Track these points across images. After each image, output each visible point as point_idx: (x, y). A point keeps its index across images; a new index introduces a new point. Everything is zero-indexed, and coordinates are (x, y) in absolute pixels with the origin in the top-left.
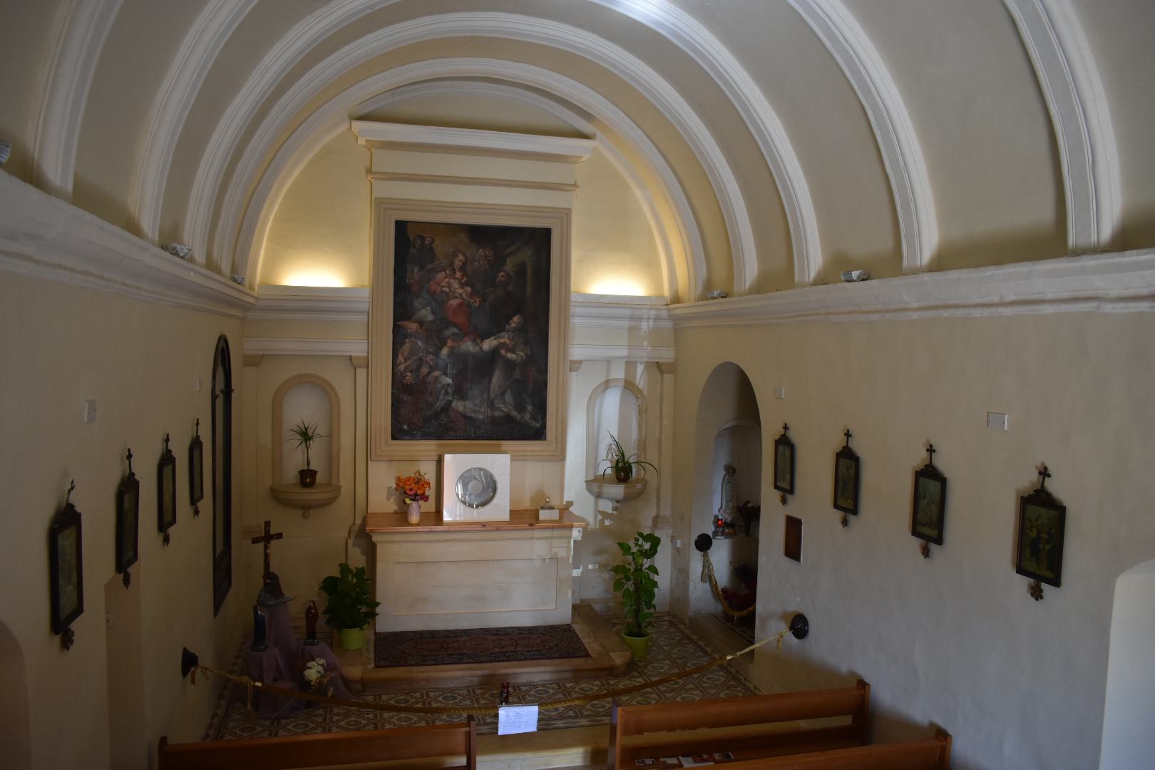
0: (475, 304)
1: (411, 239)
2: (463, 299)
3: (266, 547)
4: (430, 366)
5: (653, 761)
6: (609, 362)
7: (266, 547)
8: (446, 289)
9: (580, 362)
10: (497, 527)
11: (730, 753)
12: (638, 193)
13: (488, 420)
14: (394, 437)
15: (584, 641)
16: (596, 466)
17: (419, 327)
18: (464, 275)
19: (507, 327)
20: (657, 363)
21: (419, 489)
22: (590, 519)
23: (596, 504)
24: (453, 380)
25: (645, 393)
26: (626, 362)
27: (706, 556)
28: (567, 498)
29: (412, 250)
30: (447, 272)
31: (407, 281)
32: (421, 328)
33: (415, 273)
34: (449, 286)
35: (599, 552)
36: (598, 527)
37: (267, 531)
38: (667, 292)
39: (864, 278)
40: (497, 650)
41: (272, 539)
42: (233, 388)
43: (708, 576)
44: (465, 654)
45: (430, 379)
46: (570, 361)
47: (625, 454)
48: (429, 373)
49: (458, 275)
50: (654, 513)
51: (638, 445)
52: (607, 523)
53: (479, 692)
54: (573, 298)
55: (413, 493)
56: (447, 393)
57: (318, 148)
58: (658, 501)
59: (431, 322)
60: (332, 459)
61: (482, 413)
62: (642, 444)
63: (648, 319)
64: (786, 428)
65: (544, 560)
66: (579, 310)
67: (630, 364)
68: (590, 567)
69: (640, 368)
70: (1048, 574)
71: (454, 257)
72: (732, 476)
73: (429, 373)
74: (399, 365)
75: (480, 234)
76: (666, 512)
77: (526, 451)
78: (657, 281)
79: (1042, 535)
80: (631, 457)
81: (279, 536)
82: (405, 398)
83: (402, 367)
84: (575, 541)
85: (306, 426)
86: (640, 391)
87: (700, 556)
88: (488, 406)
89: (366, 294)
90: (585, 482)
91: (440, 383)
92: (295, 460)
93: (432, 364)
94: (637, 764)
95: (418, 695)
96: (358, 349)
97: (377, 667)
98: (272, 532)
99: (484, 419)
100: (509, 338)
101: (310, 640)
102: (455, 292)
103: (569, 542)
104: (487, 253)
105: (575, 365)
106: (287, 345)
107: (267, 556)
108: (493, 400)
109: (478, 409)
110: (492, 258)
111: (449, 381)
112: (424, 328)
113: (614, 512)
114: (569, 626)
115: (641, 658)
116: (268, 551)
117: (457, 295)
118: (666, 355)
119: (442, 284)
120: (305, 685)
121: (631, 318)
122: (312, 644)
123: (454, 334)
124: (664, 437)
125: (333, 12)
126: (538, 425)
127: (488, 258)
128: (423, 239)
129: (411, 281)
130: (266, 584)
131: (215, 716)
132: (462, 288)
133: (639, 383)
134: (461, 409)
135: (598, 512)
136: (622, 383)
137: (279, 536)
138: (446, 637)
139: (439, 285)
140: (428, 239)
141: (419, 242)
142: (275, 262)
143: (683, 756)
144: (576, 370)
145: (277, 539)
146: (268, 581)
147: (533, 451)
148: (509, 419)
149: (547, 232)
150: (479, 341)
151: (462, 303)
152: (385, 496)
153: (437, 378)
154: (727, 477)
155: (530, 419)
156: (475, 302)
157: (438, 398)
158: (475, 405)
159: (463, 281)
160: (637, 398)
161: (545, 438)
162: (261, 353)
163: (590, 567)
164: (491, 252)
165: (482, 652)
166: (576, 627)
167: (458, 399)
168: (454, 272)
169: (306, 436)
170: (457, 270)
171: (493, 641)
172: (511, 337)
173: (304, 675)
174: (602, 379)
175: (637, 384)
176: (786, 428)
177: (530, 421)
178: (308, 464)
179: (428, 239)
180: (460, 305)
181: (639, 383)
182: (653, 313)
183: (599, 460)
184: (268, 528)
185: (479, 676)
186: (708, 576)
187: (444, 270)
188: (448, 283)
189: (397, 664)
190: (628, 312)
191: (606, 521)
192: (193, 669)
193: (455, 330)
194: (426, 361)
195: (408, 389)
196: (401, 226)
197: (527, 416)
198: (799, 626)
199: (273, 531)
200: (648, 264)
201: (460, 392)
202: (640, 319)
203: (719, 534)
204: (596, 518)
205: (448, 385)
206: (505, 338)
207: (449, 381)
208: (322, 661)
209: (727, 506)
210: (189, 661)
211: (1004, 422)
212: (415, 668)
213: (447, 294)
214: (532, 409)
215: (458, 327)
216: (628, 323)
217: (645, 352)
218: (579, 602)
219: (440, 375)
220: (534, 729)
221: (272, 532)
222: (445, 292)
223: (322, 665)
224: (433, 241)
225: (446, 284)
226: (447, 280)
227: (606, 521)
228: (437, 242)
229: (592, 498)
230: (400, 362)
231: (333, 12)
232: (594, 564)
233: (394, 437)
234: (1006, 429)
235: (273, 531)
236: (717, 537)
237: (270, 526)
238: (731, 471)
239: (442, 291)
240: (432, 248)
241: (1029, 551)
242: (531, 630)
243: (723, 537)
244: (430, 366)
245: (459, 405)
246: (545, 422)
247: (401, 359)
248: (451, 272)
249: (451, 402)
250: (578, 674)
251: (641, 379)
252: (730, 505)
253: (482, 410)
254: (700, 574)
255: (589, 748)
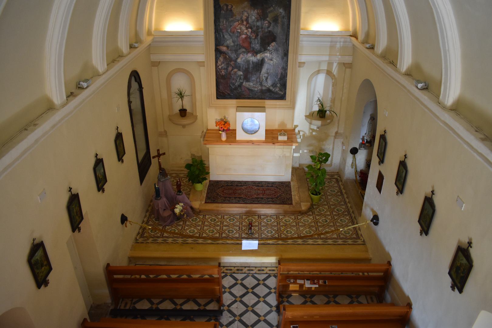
0: (253, 37)
1: (222, 6)
2: (247, 35)
4: (233, 67)
5: (294, 281)
6: (320, 63)
8: (239, 31)
9: (304, 63)
10: (259, 143)
11: (327, 281)
13: (259, 91)
17: (227, 49)
18: (248, 23)
21: (225, 127)
23: (310, 126)
28: (295, 123)
29: (223, 12)
30: (239, 22)
31: (221, 27)
32: (228, 49)
33: (223, 23)
34: (241, 29)
35: (310, 145)
37: (158, 153)
38: (351, 29)
39: (422, 89)
40: (255, 196)
41: (161, 156)
43: (354, 164)
44: (242, 198)
46: (299, 63)
48: (232, 70)
49: (245, 23)
51: (331, 100)
52: (314, 133)
53: (244, 217)
54: (302, 32)
55: (222, 129)
56: (240, 79)
58: (338, 123)
59: (232, 46)
60: (193, 104)
61: (257, 88)
62: (333, 101)
63: (340, 42)
64: (385, 132)
65: (280, 157)
66: (305, 39)
67: (330, 64)
68: (305, 151)
69: (335, 65)
70: (459, 285)
71: (242, 14)
72: (372, 121)
73: (232, 70)
76: (341, 131)
77: (276, 105)
78: (346, 23)
79: (461, 268)
80: (327, 108)
81: (164, 154)
84: (293, 149)
85: (181, 91)
86: (334, 75)
87: (352, 156)
89: (202, 33)
90: (305, 116)
91: (237, 74)
92: (177, 105)
94: (287, 282)
95: (220, 217)
97: (205, 203)
98: (161, 153)
99: (257, 90)
103: (291, 150)
104: (258, 11)
105: (302, 64)
106: (168, 57)
107: (159, 162)
109: (255, 86)
110: (261, 14)
112: (229, 49)
113: (318, 129)
115: (316, 203)
116: (160, 161)
117: (244, 33)
118: (348, 59)
119: (237, 28)
120: (174, 214)
122: (179, 195)
124: (343, 98)
126: (282, 93)
127: (259, 14)
128: (227, 6)
129: (222, 27)
130: (160, 172)
131: (146, 216)
132: (247, 30)
134: (247, 86)
136: (325, 71)
137: (164, 154)
138: (237, 186)
140: (230, 6)
141: (225, 7)
143: (307, 280)
146: (161, 171)
147: (280, 105)
148: (269, 90)
150: (255, 55)
151: (247, 37)
153: (236, 72)
154: (370, 121)
155: (279, 90)
156: (253, 36)
157: (236, 81)
159: (247, 26)
160: (332, 79)
162: (159, 61)
163: (305, 151)
164: (261, 11)
165: (249, 197)
166: (292, 184)
167: (246, 82)
168: (243, 22)
170: (244, 21)
171: (255, 190)
173: (174, 211)
174: (317, 69)
175: (333, 72)
176: (385, 132)
177: (278, 91)
178: (183, 107)
179: (230, 6)
180: (246, 38)
181: (334, 72)
182: (342, 40)
184: (159, 152)
185: (245, 210)
187: (238, 21)
189: (214, 202)
190: (329, 39)
191: (313, 133)
192: (126, 222)
193: (244, 50)
195: (223, 77)
197: (277, 90)
198: (376, 219)
200: (343, 13)
201: (247, 79)
202: (336, 42)
203: (363, 147)
205: (241, 75)
208: (182, 204)
209: (368, 134)
210: (124, 219)
211: (462, 206)
212: (220, 205)
213: (240, 33)
214: (280, 86)
215: (245, 49)
217: (337, 59)
218: (298, 166)
219: (237, 71)
220: (257, 248)
221: (161, 153)
222: (239, 32)
223: (182, 206)
224: (232, 7)
226: (239, 26)
227: (313, 133)
228: (234, 7)
229: (308, 124)
230: (219, 65)
232: (307, 150)
233: (217, 98)
234: (462, 210)
236: (361, 149)
237: (159, 151)
238: (372, 119)
239: (237, 31)
240: (232, 10)
241: (455, 269)
242: (273, 183)
243: (364, 149)
244: (233, 67)
245: (246, 84)
246: (286, 92)
247: (219, 63)
249: (242, 83)
250: (286, 213)
252: (370, 133)
255: (278, 258)
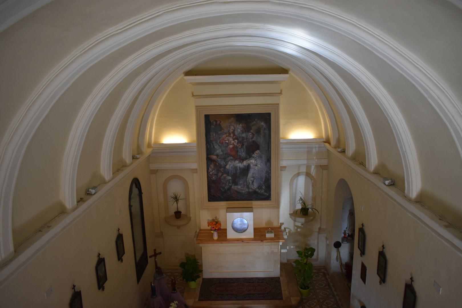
0: (239, 147)
1: (211, 122)
3: (155, 259)
4: (222, 173)
6: (299, 166)
7: (155, 259)
8: (227, 142)
9: (285, 167)
10: (248, 240)
12: (310, 93)
14: (209, 201)
15: (282, 289)
16: (295, 206)
17: (217, 157)
18: (234, 135)
19: (253, 155)
20: (321, 165)
22: (292, 229)
23: (294, 223)
24: (231, 177)
25: (315, 177)
26: (307, 166)
27: (338, 252)
29: (213, 127)
30: (227, 134)
32: (218, 157)
33: (213, 135)
36: (295, 232)
37: (155, 253)
38: (324, 136)
42: (142, 192)
43: (339, 258)
45: (222, 177)
46: (281, 167)
47: (306, 203)
49: (232, 135)
50: (319, 226)
52: (299, 230)
54: (281, 141)
55: (214, 229)
56: (229, 182)
57: (171, 87)
60: (187, 206)
61: (245, 190)
62: (314, 199)
67: (308, 167)
68: (292, 247)
69: (313, 167)
74: (210, 173)
75: (240, 118)
81: (160, 253)
82: (213, 185)
83: (211, 173)
84: (280, 245)
85: (176, 195)
86: (313, 177)
88: (246, 187)
89: (195, 144)
90: (289, 214)
92: (173, 208)
93: (223, 172)
96: (194, 166)
97: (199, 300)
99: (245, 192)
100: (254, 160)
101: (173, 291)
102: (231, 142)
103: (279, 247)
104: (243, 125)
105: (283, 168)
108: (248, 185)
109: (242, 189)
111: (230, 178)
112: (219, 157)
113: (302, 226)
114: (279, 278)
116: (156, 260)
117: (232, 143)
118: (324, 162)
119: (225, 139)
121: (308, 148)
122: (174, 293)
123: (231, 159)
125: (149, 73)
128: (216, 121)
130: (156, 271)
132: (234, 140)
133: (313, 173)
134: (236, 189)
135: (295, 226)
136: (305, 173)
137: (160, 253)
139: (224, 140)
141: (215, 123)
142: (159, 133)
144: (284, 170)
145: (159, 254)
148: (255, 192)
149: (269, 114)
152: (207, 225)
153: (225, 177)
154: (350, 216)
157: (226, 185)
158: (241, 187)
159: (234, 137)
160: (312, 180)
161: (271, 199)
163: (292, 247)
167: (234, 185)
168: (230, 134)
169: (176, 199)
170: (231, 133)
172: (255, 159)
174: (297, 172)
175: (311, 174)
177: (264, 193)
179: (218, 121)
180: (233, 148)
181: (313, 173)
182: (317, 146)
183: (296, 203)
186: (339, 258)
187: (226, 134)
188: (228, 139)
190: (306, 146)
193: (232, 158)
194: (220, 171)
196: (207, 117)
197: (263, 191)
199: (157, 252)
200: (315, 124)
203: (345, 241)
204: (294, 228)
205: (230, 180)
206: (253, 161)
207: (230, 178)
208: (177, 302)
209: (349, 228)
212: (213, 302)
216: (306, 149)
218: (286, 262)
222: (227, 143)
223: (177, 304)
224: (221, 122)
225: (227, 139)
226: (227, 138)
228: (222, 122)
231: (149, 73)
232: (294, 246)
233: (209, 201)
234: (440, 293)
235: (157, 252)
236: (344, 242)
237: (156, 251)
239: (225, 142)
240: (220, 125)
242: (263, 279)
244: (222, 173)
245: (234, 187)
248: (229, 134)
249: (231, 186)
251: (313, 171)
253: (244, 189)
254: (336, 257)
